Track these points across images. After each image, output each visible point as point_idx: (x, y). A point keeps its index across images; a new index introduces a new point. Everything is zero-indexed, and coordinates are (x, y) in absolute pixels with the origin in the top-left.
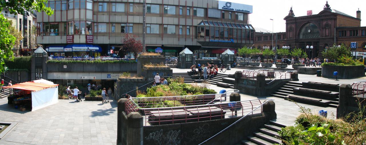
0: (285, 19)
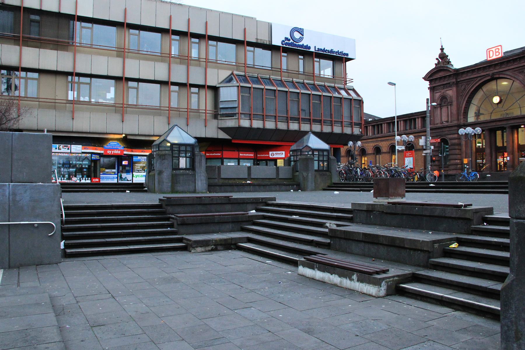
0: (425, 78)
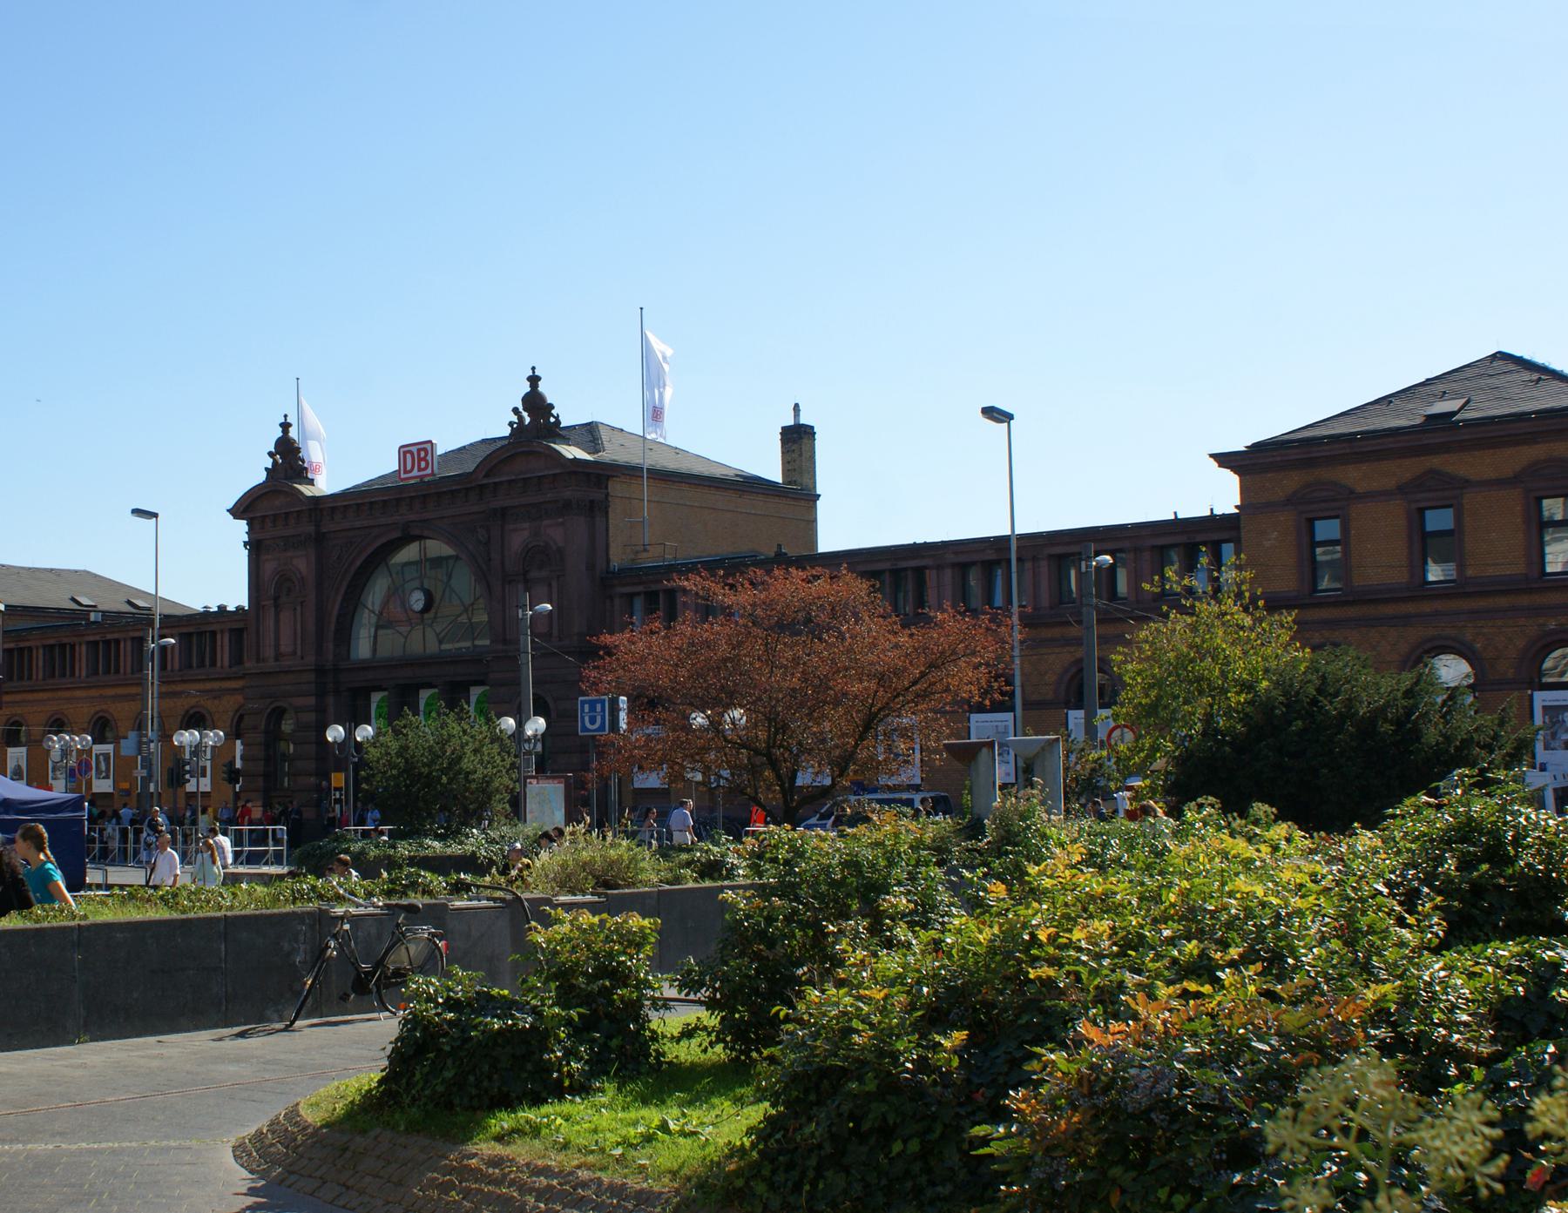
0: (238, 511)
